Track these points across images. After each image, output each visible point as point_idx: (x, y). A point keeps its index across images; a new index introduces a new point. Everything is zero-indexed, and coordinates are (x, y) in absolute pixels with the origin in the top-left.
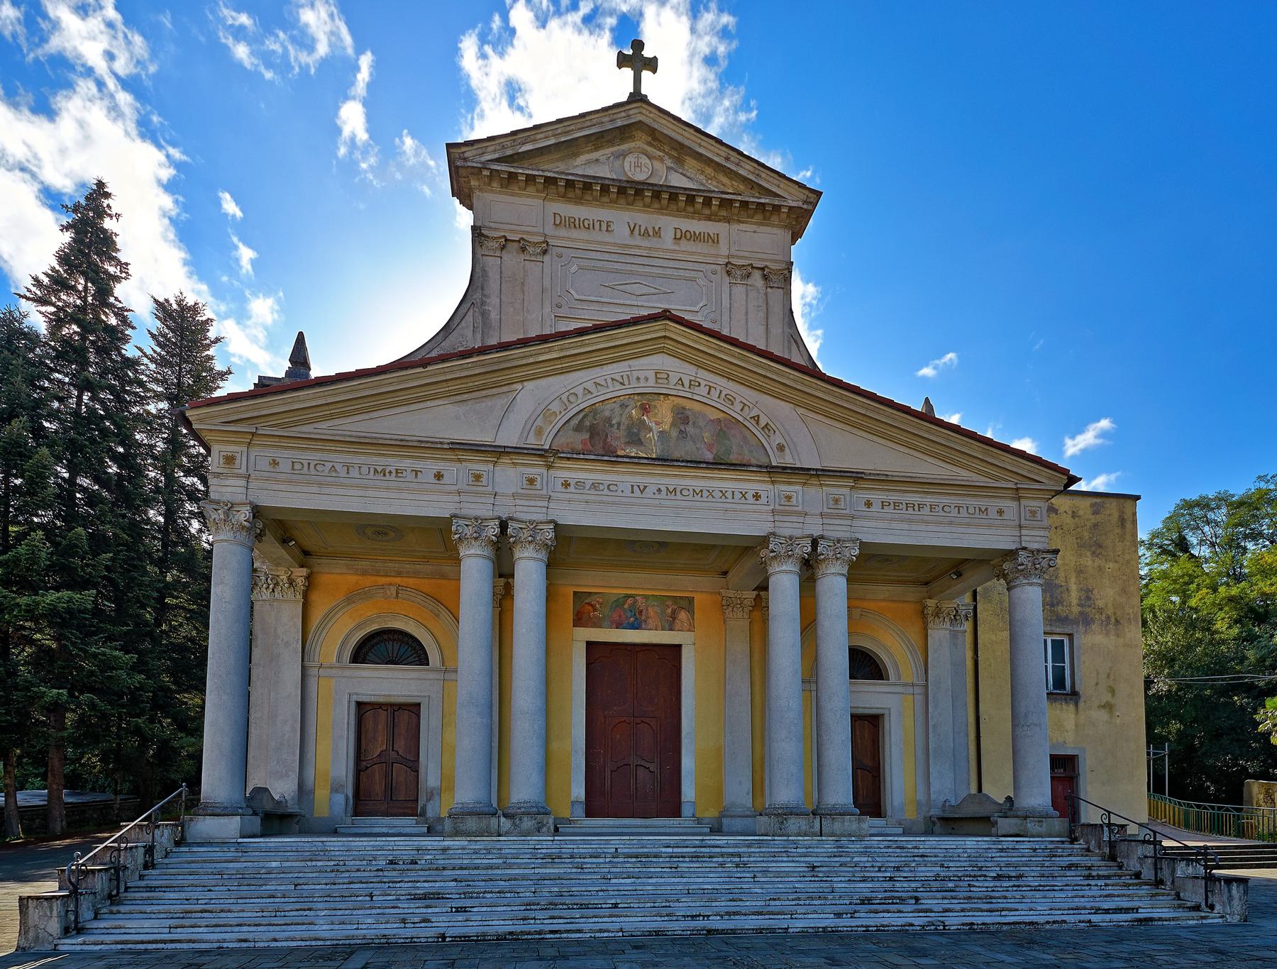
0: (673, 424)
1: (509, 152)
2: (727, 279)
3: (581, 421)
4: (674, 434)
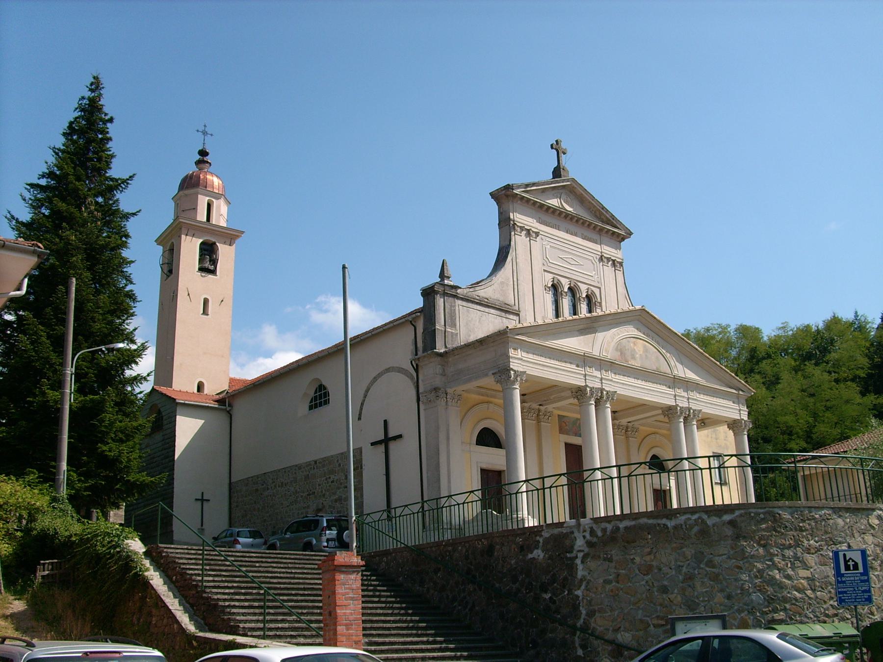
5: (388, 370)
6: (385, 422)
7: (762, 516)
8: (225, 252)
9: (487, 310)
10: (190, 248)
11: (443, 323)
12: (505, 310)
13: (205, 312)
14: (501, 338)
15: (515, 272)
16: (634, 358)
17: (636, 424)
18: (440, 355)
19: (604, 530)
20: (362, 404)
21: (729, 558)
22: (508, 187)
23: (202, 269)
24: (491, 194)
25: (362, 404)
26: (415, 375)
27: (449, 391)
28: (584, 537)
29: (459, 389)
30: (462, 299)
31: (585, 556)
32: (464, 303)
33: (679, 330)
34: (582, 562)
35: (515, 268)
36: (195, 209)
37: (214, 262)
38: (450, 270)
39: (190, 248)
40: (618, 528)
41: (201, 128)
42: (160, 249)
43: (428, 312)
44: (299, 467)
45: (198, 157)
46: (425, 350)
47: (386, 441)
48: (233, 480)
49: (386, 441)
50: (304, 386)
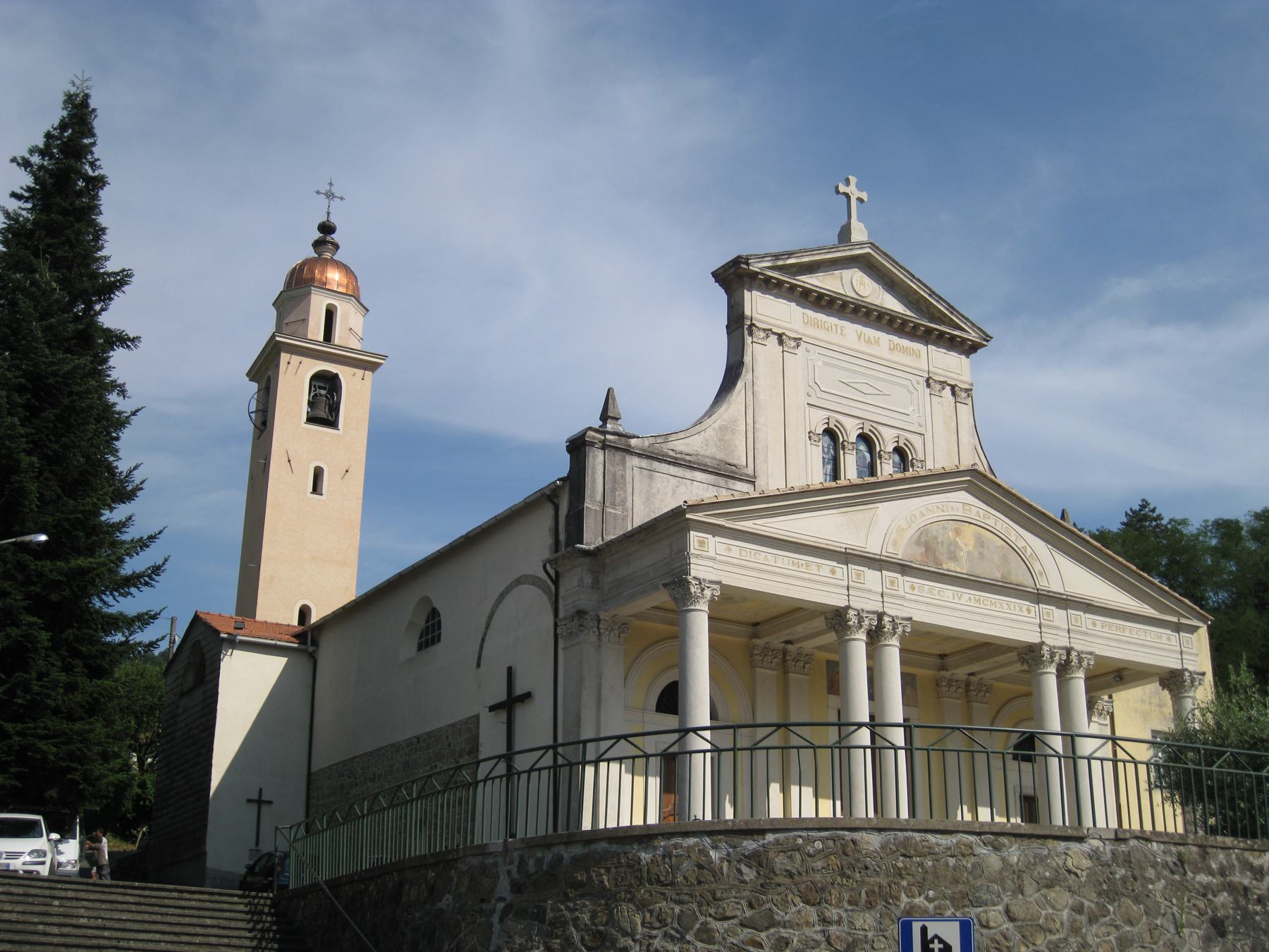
4: (976, 554)
5: (519, 581)
6: (510, 669)
7: (819, 845)
8: (356, 391)
9: (689, 474)
10: (295, 380)
11: (599, 497)
12: (725, 471)
13: (316, 488)
14: (673, 525)
15: (752, 409)
16: (953, 557)
17: (987, 676)
18: (586, 553)
19: (539, 862)
20: (483, 640)
21: (742, 925)
22: (737, 262)
23: (311, 420)
24: (714, 274)
25: (483, 640)
26: (553, 588)
27: (603, 616)
28: (509, 872)
29: (626, 611)
30: (639, 455)
31: (505, 912)
32: (644, 463)
34: (501, 921)
35: (750, 402)
36: (305, 321)
37: (334, 408)
38: (622, 404)
39: (295, 380)
40: (560, 859)
42: (254, 387)
43: (576, 481)
44: (396, 747)
45: (318, 235)
46: (567, 545)
47: (511, 703)
48: (313, 770)
49: (511, 703)
50: (405, 610)
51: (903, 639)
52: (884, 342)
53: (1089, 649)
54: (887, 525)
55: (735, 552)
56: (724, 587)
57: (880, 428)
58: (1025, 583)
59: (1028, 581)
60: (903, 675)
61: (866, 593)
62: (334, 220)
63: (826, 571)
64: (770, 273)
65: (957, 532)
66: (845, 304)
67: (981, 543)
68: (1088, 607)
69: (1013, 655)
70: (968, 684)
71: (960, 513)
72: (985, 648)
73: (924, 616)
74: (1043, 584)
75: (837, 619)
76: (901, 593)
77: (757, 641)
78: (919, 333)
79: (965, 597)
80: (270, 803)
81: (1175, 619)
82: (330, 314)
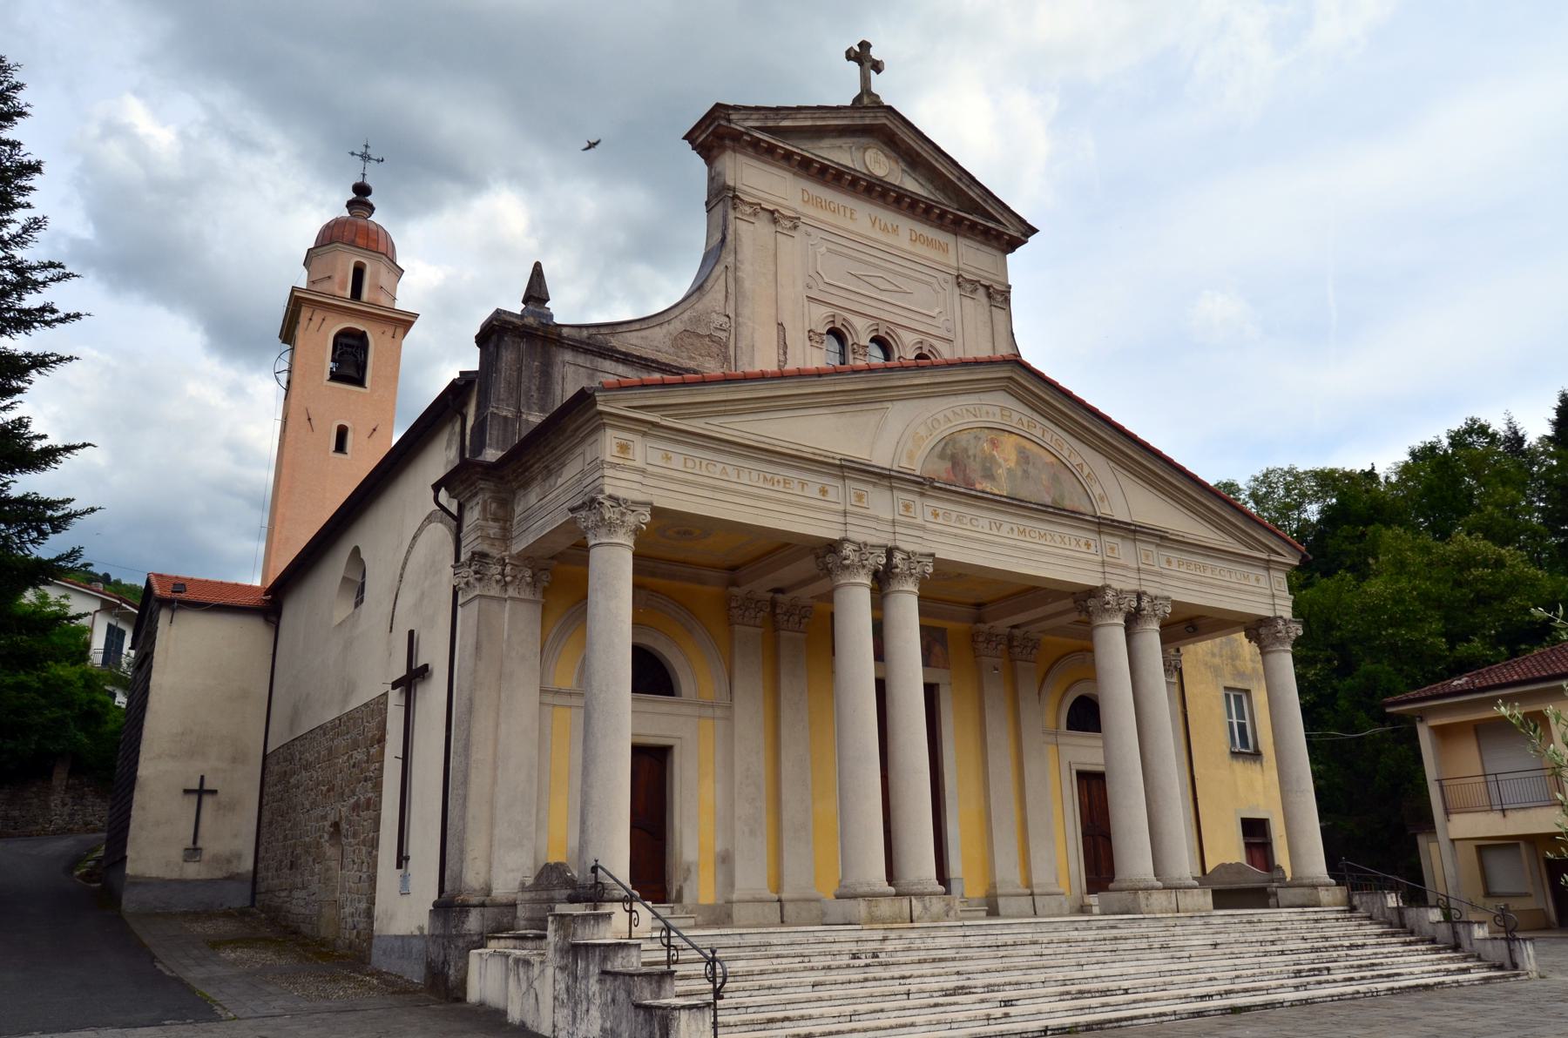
0: (1017, 463)
1: (770, 124)
2: (957, 291)
3: (944, 449)
4: (1019, 473)
6: (411, 633)
16: (989, 476)
23: (335, 377)
33: (1212, 482)
35: (731, 289)
37: (361, 367)
41: (360, 150)
47: (414, 677)
49: (414, 677)
51: (923, 582)
52: (904, 232)
53: (1166, 594)
54: (898, 433)
55: (677, 462)
56: (657, 512)
57: (900, 331)
58: (1082, 510)
59: (1084, 507)
60: (924, 629)
61: (873, 520)
62: (369, 182)
63: (813, 490)
64: (758, 135)
65: (994, 444)
66: (854, 182)
67: (1024, 458)
68: (1161, 538)
69: (1069, 603)
70: (1011, 638)
71: (996, 419)
72: (1033, 592)
73: (950, 551)
74: (1104, 510)
75: (826, 552)
76: (919, 521)
77: (735, 590)
78: (947, 221)
79: (1006, 527)
80: (214, 792)
81: (1264, 556)
82: (359, 272)
